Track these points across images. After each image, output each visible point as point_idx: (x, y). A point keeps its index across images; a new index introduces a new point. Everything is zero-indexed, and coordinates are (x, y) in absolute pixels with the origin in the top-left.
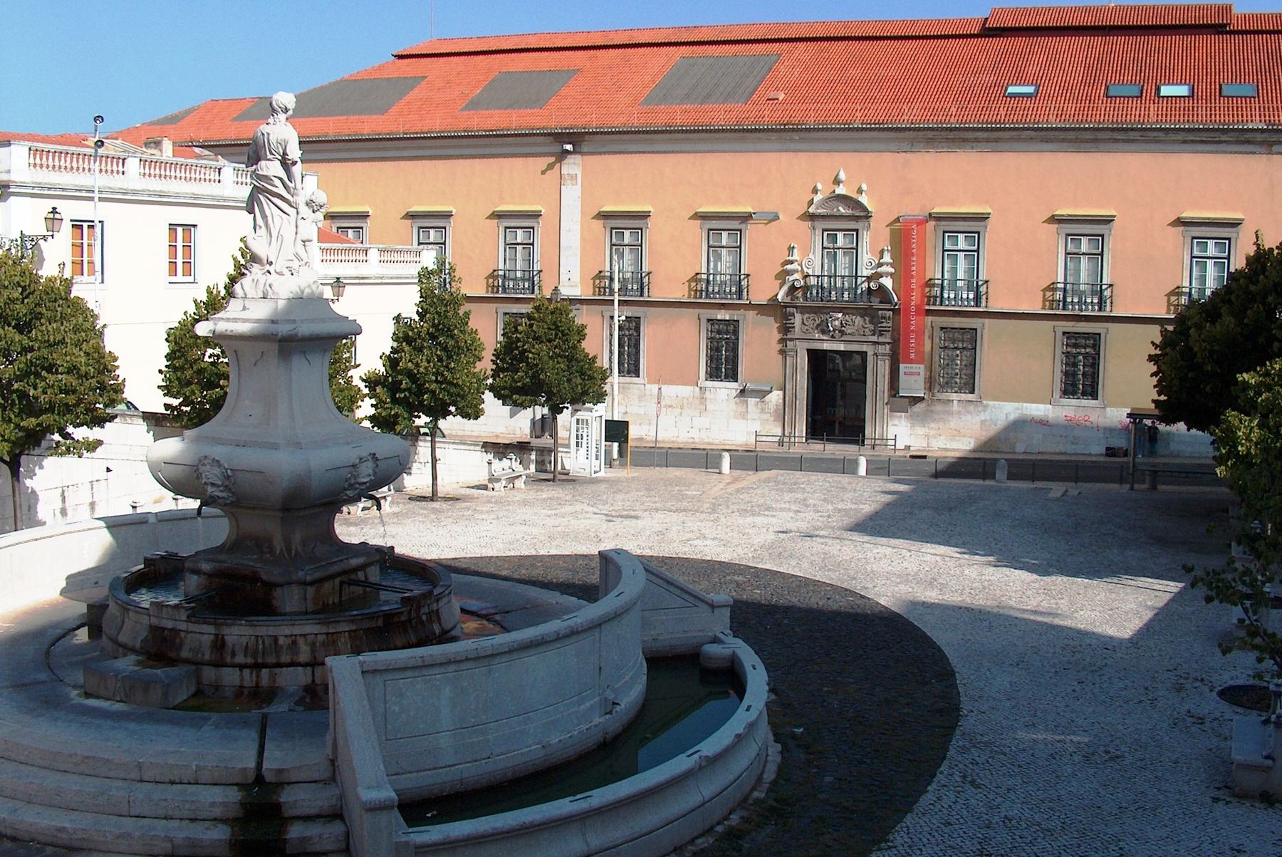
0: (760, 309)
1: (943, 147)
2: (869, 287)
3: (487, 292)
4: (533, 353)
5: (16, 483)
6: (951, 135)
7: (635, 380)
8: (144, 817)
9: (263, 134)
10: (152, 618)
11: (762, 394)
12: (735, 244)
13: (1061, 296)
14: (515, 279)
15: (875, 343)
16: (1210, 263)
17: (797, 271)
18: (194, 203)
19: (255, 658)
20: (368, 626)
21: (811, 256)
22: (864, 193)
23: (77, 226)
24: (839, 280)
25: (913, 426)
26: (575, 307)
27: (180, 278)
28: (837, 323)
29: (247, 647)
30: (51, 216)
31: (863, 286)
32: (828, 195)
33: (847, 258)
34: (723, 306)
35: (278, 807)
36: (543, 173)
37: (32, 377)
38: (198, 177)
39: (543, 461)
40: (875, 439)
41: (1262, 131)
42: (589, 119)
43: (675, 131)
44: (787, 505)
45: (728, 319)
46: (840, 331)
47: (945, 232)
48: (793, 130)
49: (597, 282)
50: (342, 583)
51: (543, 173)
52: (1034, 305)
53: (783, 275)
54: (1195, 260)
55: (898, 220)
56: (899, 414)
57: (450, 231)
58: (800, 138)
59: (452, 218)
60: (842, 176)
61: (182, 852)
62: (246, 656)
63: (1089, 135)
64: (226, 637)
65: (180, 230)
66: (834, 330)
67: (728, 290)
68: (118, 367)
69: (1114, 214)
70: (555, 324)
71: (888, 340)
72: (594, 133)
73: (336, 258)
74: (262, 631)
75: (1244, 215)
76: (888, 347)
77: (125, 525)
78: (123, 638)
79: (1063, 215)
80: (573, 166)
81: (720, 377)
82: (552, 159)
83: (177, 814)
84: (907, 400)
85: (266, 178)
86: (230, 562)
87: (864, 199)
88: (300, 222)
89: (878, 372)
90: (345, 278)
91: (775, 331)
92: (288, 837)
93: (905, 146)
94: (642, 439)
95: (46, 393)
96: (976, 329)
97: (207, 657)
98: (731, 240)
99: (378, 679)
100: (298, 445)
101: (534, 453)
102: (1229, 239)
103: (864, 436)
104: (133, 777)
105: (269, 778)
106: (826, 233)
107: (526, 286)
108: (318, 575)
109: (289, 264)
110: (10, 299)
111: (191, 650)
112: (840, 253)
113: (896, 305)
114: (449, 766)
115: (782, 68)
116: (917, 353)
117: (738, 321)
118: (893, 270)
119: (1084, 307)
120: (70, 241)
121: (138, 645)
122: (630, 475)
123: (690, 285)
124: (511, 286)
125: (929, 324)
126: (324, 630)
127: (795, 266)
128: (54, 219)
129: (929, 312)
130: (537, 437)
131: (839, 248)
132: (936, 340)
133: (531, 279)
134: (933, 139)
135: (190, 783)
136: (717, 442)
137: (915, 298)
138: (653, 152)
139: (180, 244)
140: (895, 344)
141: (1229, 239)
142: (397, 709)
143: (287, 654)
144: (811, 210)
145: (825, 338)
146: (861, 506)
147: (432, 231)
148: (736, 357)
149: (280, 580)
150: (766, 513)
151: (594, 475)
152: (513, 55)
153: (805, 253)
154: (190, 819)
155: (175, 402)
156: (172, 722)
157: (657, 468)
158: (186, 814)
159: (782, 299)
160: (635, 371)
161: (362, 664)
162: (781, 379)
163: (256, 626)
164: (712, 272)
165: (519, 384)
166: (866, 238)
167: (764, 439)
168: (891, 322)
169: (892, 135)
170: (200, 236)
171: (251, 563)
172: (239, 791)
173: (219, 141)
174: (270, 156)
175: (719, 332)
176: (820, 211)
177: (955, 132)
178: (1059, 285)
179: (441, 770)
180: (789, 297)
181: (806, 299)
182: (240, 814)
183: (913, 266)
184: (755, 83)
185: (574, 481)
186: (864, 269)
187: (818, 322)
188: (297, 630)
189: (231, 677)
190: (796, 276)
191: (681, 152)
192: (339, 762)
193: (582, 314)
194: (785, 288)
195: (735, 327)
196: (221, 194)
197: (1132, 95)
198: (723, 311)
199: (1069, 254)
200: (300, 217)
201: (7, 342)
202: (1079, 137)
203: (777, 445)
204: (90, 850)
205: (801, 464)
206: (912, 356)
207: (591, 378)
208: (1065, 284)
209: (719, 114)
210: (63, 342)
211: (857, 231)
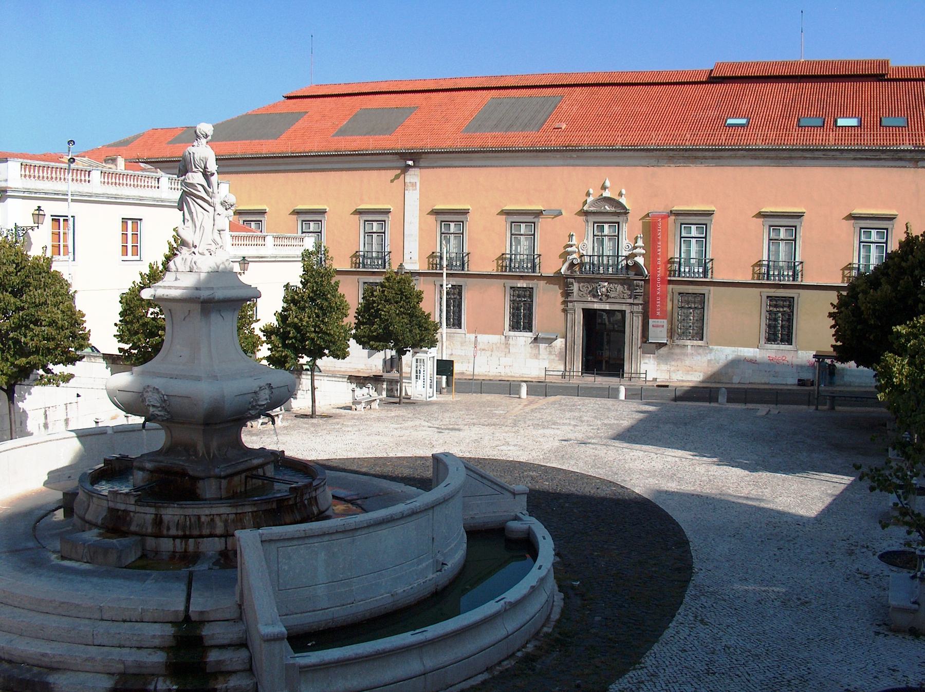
0: (549, 279)
2: (627, 264)
3: (352, 267)
5: (11, 405)
8: (104, 646)
9: (190, 154)
11: (550, 341)
13: (766, 270)
14: (372, 258)
15: (631, 304)
17: (575, 252)
19: (184, 531)
20: (265, 508)
21: (585, 241)
23: (56, 220)
24: (605, 259)
25: (658, 364)
27: (130, 257)
28: (604, 290)
30: (37, 212)
31: (623, 263)
33: (611, 243)
34: (522, 277)
35: (201, 638)
36: (392, 181)
37: (23, 328)
38: (143, 184)
42: (426, 142)
43: (487, 152)
46: (606, 296)
48: (572, 150)
49: (431, 260)
50: (247, 477)
51: (392, 181)
52: (491, 269)
53: (565, 255)
56: (649, 355)
58: (577, 157)
60: (608, 184)
61: (132, 671)
62: (177, 530)
64: (163, 516)
65: (130, 222)
66: (602, 295)
68: (85, 321)
70: (400, 290)
72: (428, 153)
73: (243, 243)
74: (189, 512)
76: (640, 306)
77: (90, 435)
78: (88, 517)
80: (414, 177)
82: (399, 172)
83: (128, 643)
84: (654, 345)
85: (192, 185)
86: (166, 462)
87: (623, 200)
88: (217, 217)
90: (249, 257)
91: (559, 296)
93: (653, 162)
97: (149, 530)
99: (273, 547)
100: (215, 378)
101: (385, 383)
103: (623, 371)
105: (194, 617)
106: (596, 225)
107: (380, 263)
108: (229, 471)
109: (209, 247)
110: (7, 272)
111: (137, 525)
112: (606, 239)
113: (646, 277)
114: (324, 609)
116: (662, 311)
121: (100, 522)
123: (498, 262)
124: (369, 263)
126: (234, 511)
127: (573, 249)
128: (39, 215)
136: (518, 375)
137: (660, 272)
138: (471, 166)
139: (130, 233)
140: (646, 305)
142: (286, 568)
144: (585, 208)
145: (595, 300)
149: (202, 475)
151: (428, 400)
153: (581, 240)
154: (137, 648)
155: (126, 347)
156: (126, 577)
158: (134, 643)
162: (564, 330)
164: (513, 253)
165: (374, 334)
166: (625, 228)
167: (551, 373)
168: (643, 289)
169: (643, 154)
170: (144, 227)
172: (173, 627)
173: (158, 158)
174: (195, 170)
181: (581, 272)
182: (174, 644)
185: (414, 403)
188: (214, 511)
189: (166, 545)
190: (575, 256)
192: (245, 606)
194: (567, 265)
195: (530, 292)
196: (159, 197)
200: (216, 213)
201: (5, 303)
205: (578, 391)
206: (658, 313)
208: (769, 261)
210: (45, 303)
211: (618, 223)
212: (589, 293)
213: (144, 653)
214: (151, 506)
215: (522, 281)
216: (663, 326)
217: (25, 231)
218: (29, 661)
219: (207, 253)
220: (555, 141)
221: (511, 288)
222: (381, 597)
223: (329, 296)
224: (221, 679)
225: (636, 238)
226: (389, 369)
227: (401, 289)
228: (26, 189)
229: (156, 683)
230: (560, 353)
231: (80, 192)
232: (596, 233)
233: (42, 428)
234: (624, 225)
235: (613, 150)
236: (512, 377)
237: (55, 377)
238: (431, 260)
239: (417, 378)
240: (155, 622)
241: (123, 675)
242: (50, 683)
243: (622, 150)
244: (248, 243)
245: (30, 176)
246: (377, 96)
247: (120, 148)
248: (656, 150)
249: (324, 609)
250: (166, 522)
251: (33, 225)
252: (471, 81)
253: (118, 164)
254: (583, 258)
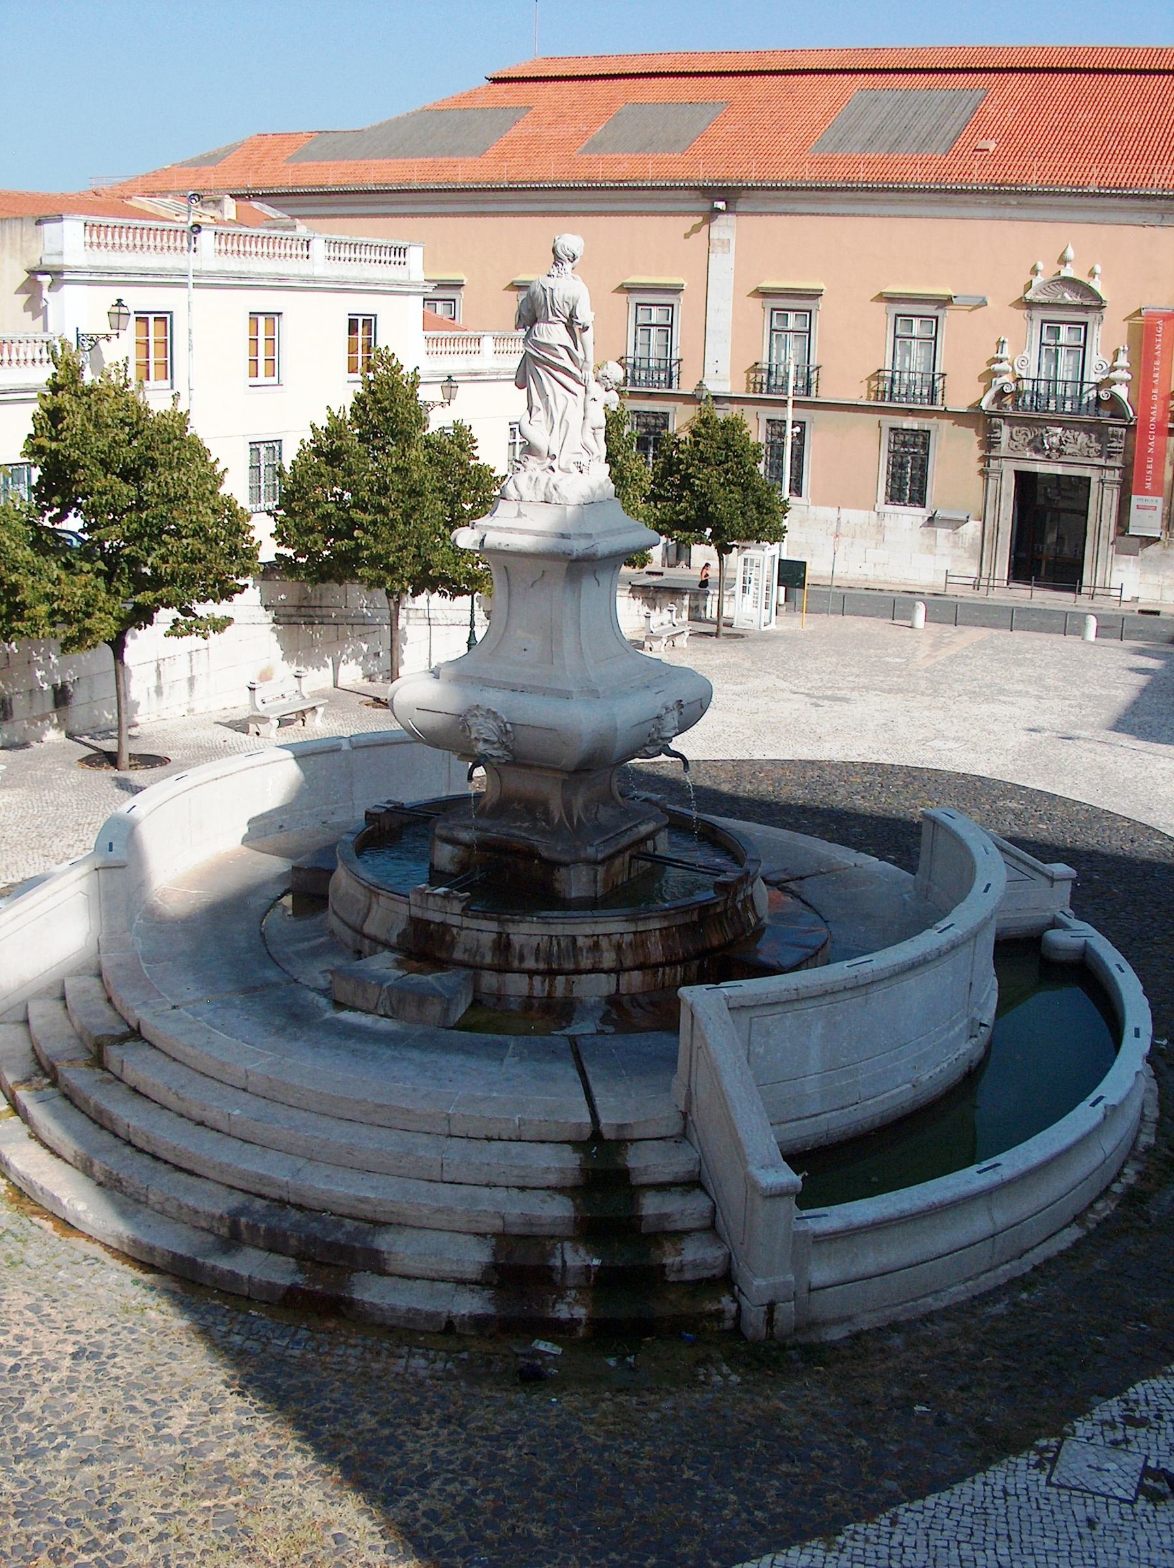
0: (958, 417)
2: (1098, 397)
4: (699, 479)
5: (120, 666)
8: (460, 1183)
9: (544, 290)
10: (413, 908)
11: (955, 524)
12: (929, 335)
14: (648, 369)
17: (1007, 372)
18: (280, 284)
19: (549, 964)
20: (682, 922)
21: (1026, 354)
23: (142, 317)
24: (1060, 386)
25: (1143, 572)
27: (262, 379)
28: (1055, 440)
29: (538, 949)
30: (116, 310)
31: (1090, 394)
33: (1071, 358)
34: (911, 412)
35: (624, 1174)
36: (687, 236)
37: (146, 539)
38: (283, 253)
39: (697, 607)
42: (748, 171)
43: (858, 189)
44: (1020, 687)
46: (1058, 450)
48: (1010, 193)
49: (752, 375)
50: (632, 857)
51: (687, 236)
52: (858, 394)
53: (989, 376)
56: (1127, 557)
58: (1019, 204)
60: (1070, 254)
61: (515, 1230)
62: (537, 960)
64: (511, 937)
65: (261, 319)
66: (1051, 449)
68: (252, 527)
70: (726, 442)
71: (1119, 464)
72: (753, 188)
73: (444, 349)
74: (558, 930)
76: (1117, 472)
77: (313, 754)
78: (370, 928)
80: (725, 228)
82: (699, 219)
83: (502, 1180)
84: (1138, 540)
85: (549, 347)
86: (497, 831)
87: (1097, 285)
88: (590, 404)
90: (456, 375)
91: (976, 446)
92: (644, 1213)
93: (1154, 218)
95: (167, 562)
97: (488, 960)
99: (745, 1016)
100: (595, 693)
101: (687, 597)
103: (1081, 583)
104: (439, 1130)
105: (608, 1134)
106: (1045, 326)
107: (662, 378)
108: (610, 851)
109: (577, 458)
110: (115, 441)
111: (466, 950)
112: (1063, 351)
113: (1132, 419)
114: (816, 1115)
115: (991, 108)
116: (1154, 483)
118: (1129, 377)
120: (134, 338)
121: (394, 940)
122: (805, 629)
123: (869, 385)
124: (643, 378)
126: (632, 928)
127: (1004, 366)
128: (119, 314)
130: (670, 566)
135: (510, 1140)
136: (897, 581)
137: (1155, 414)
138: (828, 215)
139: (261, 337)
140: (1127, 470)
142: (762, 1050)
143: (587, 958)
144: (1029, 296)
145: (1038, 457)
146: (1113, 692)
149: (566, 858)
150: (1002, 698)
151: (764, 629)
152: (641, 81)
153: (1018, 350)
154: (518, 1188)
155: (289, 552)
156: (464, 1050)
157: (833, 617)
158: (513, 1181)
161: (727, 999)
162: (980, 506)
163: (549, 923)
164: (898, 368)
165: (681, 517)
166: (1096, 335)
167: (955, 580)
168: (1123, 442)
169: (1138, 203)
170: (287, 326)
171: (523, 834)
172: (575, 1151)
173: (272, 188)
174: (552, 318)
176: (1041, 298)
179: (806, 1121)
181: (1016, 407)
182: (580, 1182)
184: (956, 128)
185: (743, 637)
188: (600, 929)
189: (517, 985)
190: (1006, 378)
191: (863, 215)
192: (694, 1116)
194: (991, 394)
195: (924, 438)
196: (310, 273)
200: (590, 397)
201: (113, 497)
204: (399, 1224)
205: (1013, 619)
206: (1148, 486)
207: (770, 511)
210: (185, 496)
211: (1086, 324)
212: (1029, 444)
213: (532, 1198)
214: (491, 919)
215: (910, 418)
216: (1155, 509)
217: (94, 340)
218: (334, 1208)
219: (574, 468)
220: (978, 177)
221: (892, 429)
222: (898, 1090)
223: (619, 458)
224: (668, 1246)
225: (1116, 353)
226: (673, 560)
227: (726, 440)
228: (94, 267)
229: (562, 1253)
230: (972, 545)
231: (180, 270)
232: (1045, 340)
233: (153, 694)
234: (1096, 328)
235: (1082, 194)
236: (886, 582)
237: (201, 624)
238: (752, 375)
239: (744, 592)
240: (542, 1142)
241: (502, 1237)
242: (383, 1252)
243: (1100, 194)
244: (452, 349)
245: (99, 245)
246: (655, 81)
247: (203, 168)
248: (1161, 197)
249: (816, 1115)
250: (518, 948)
251: (109, 331)
252: (818, 56)
253: (226, 209)
254: (1020, 383)
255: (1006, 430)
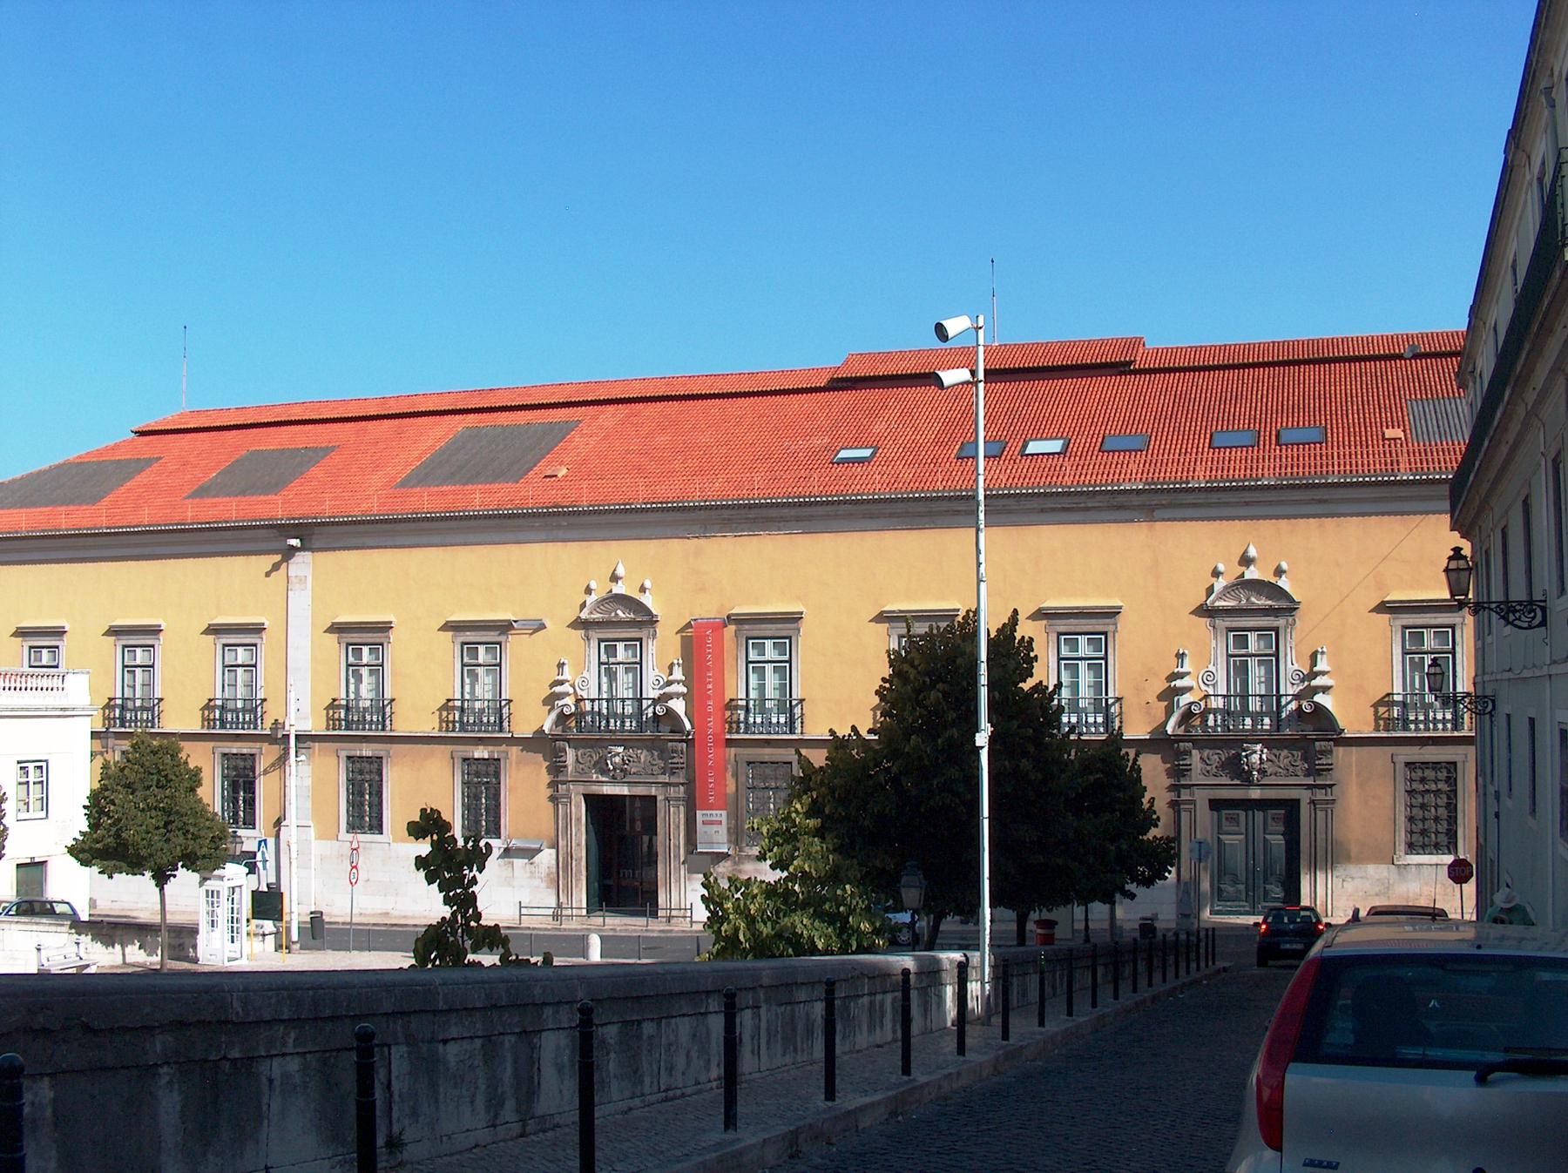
1: (743, 531)
3: (1377, 729)
6: (752, 514)
7: (377, 837)
12: (494, 662)
14: (236, 710)
15: (1309, 787)
16: (769, 668)
17: (1189, 689)
22: (647, 591)
26: (305, 745)
28: (617, 759)
32: (604, 595)
36: (268, 574)
40: (671, 909)
41: (1138, 492)
42: (326, 507)
45: (486, 757)
46: (622, 770)
47: (748, 639)
49: (331, 712)
51: (268, 574)
52: (428, 725)
54: (1063, 662)
55: (689, 625)
57: (159, 650)
59: (161, 634)
60: (621, 571)
63: (921, 507)
66: (615, 769)
67: (485, 720)
69: (1120, 604)
72: (323, 524)
75: (1122, 601)
76: (682, 788)
79: (894, 612)
80: (303, 565)
81: (363, 827)
82: (278, 558)
84: (709, 857)
87: (647, 600)
89: (671, 820)
91: (544, 771)
94: (388, 913)
96: (791, 763)
98: (490, 656)
102: (1105, 633)
113: (689, 734)
117: (499, 760)
118: (685, 690)
119: (1431, 726)
123: (441, 715)
125: (732, 756)
127: (566, 688)
129: (730, 743)
131: (619, 664)
132: (742, 779)
133: (253, 708)
134: (729, 519)
137: (713, 724)
140: (690, 784)
141: (1105, 633)
144: (584, 615)
145: (604, 779)
147: (138, 651)
148: (498, 806)
159: (551, 730)
160: (377, 826)
162: (553, 833)
166: (651, 649)
169: (678, 516)
175: (477, 775)
176: (596, 616)
177: (756, 511)
178: (740, 703)
180: (561, 727)
183: (709, 683)
186: (1289, 685)
187: (596, 758)
193: (314, 753)
194: (554, 715)
197: (1236, 445)
198: (481, 747)
199: (127, 666)
202: (910, 510)
203: (551, 918)
209: (478, 498)
211: (1277, 630)
255: (1195, 752)
